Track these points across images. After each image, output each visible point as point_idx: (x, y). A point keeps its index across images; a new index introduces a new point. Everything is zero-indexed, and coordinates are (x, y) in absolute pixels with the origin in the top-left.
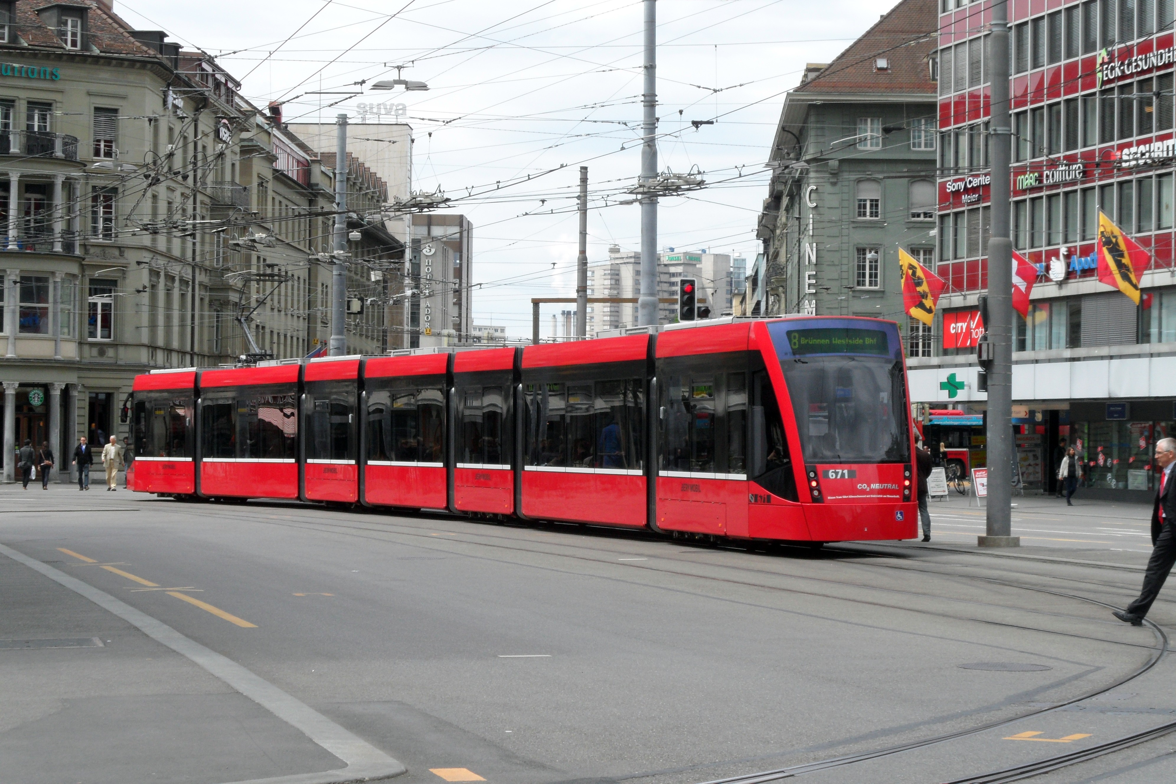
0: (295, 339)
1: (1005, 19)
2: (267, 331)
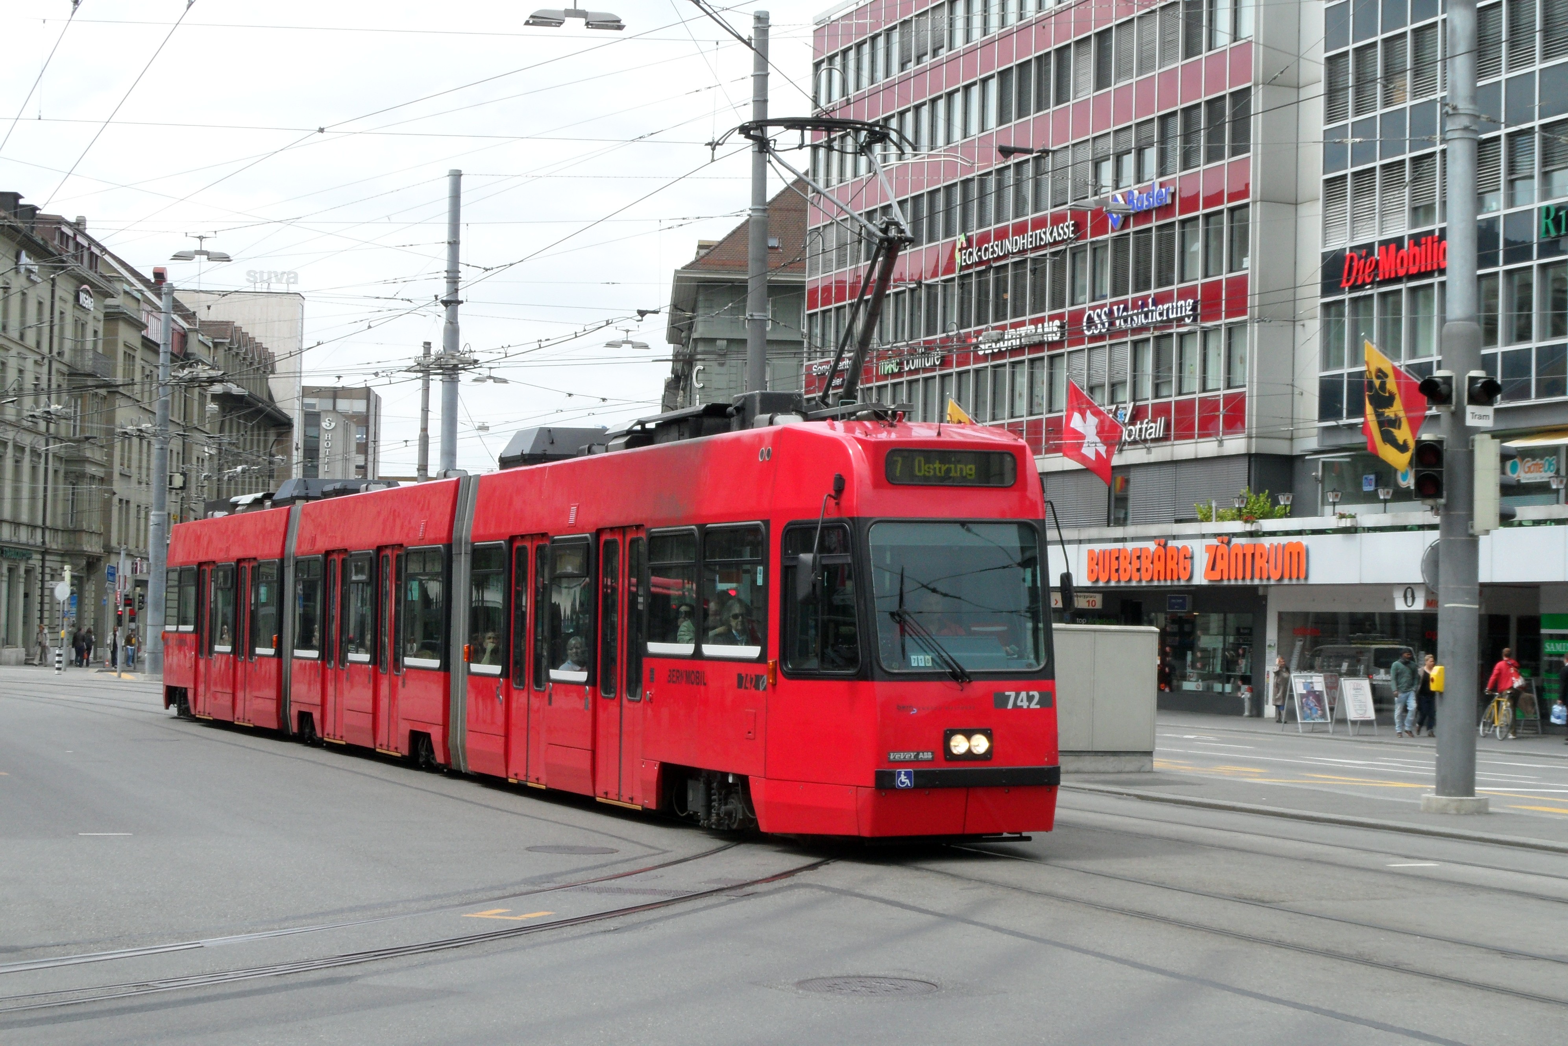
2: (133, 506)
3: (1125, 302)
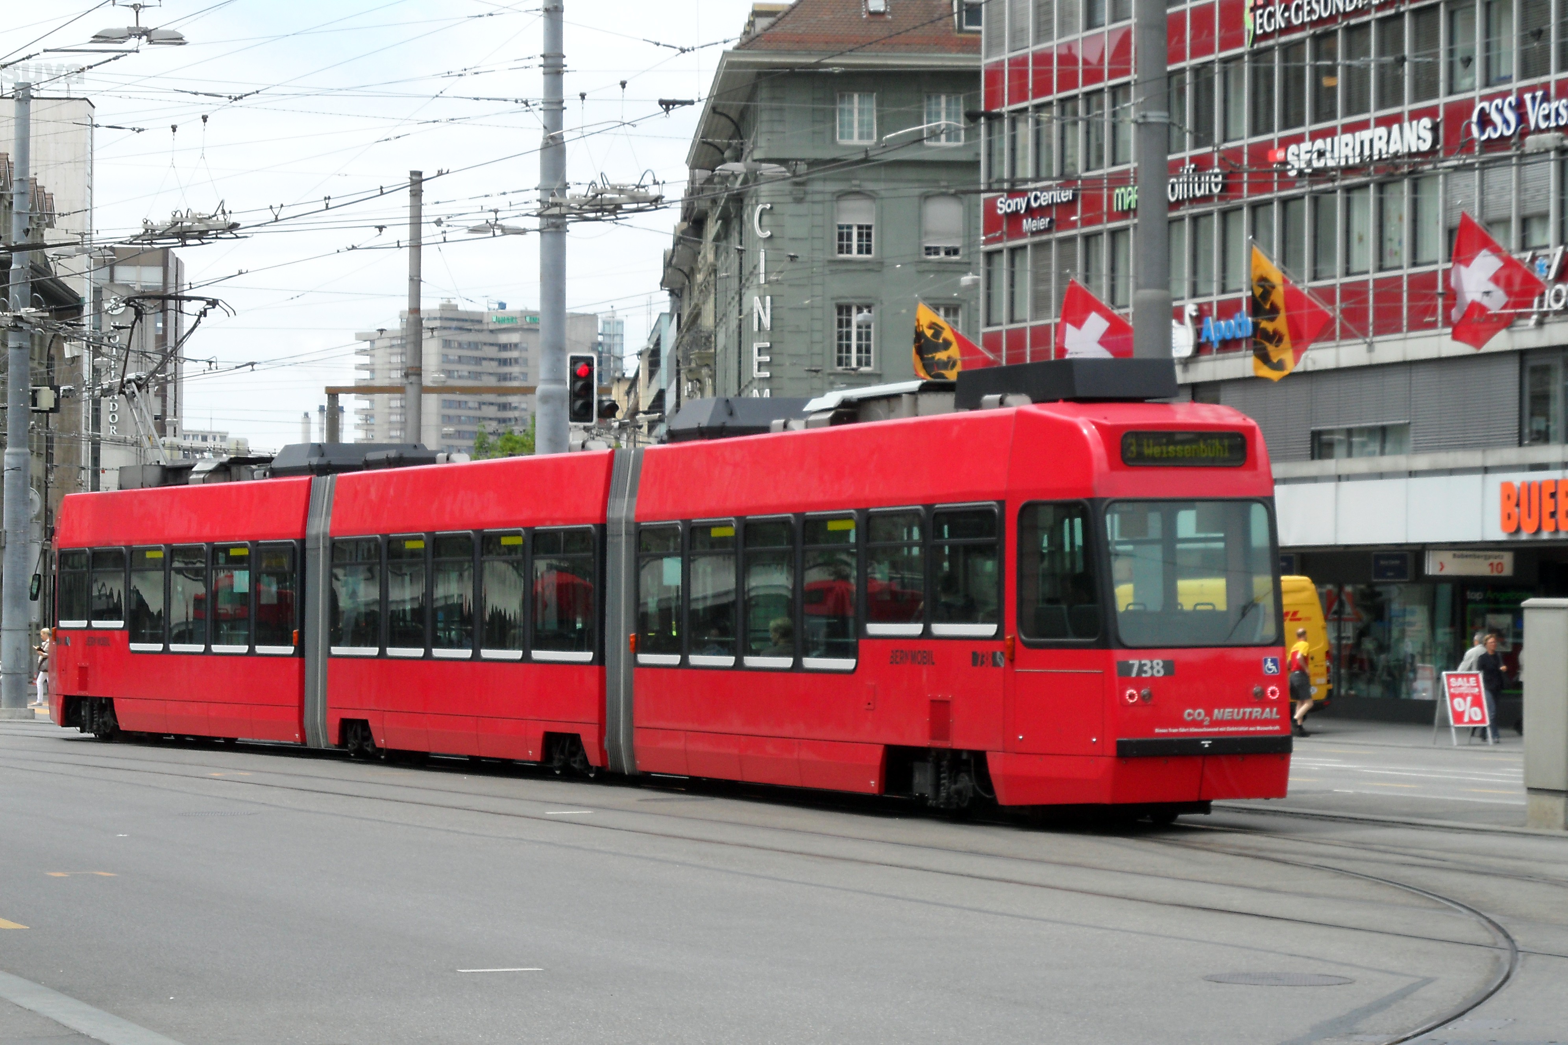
3: (1546, 87)
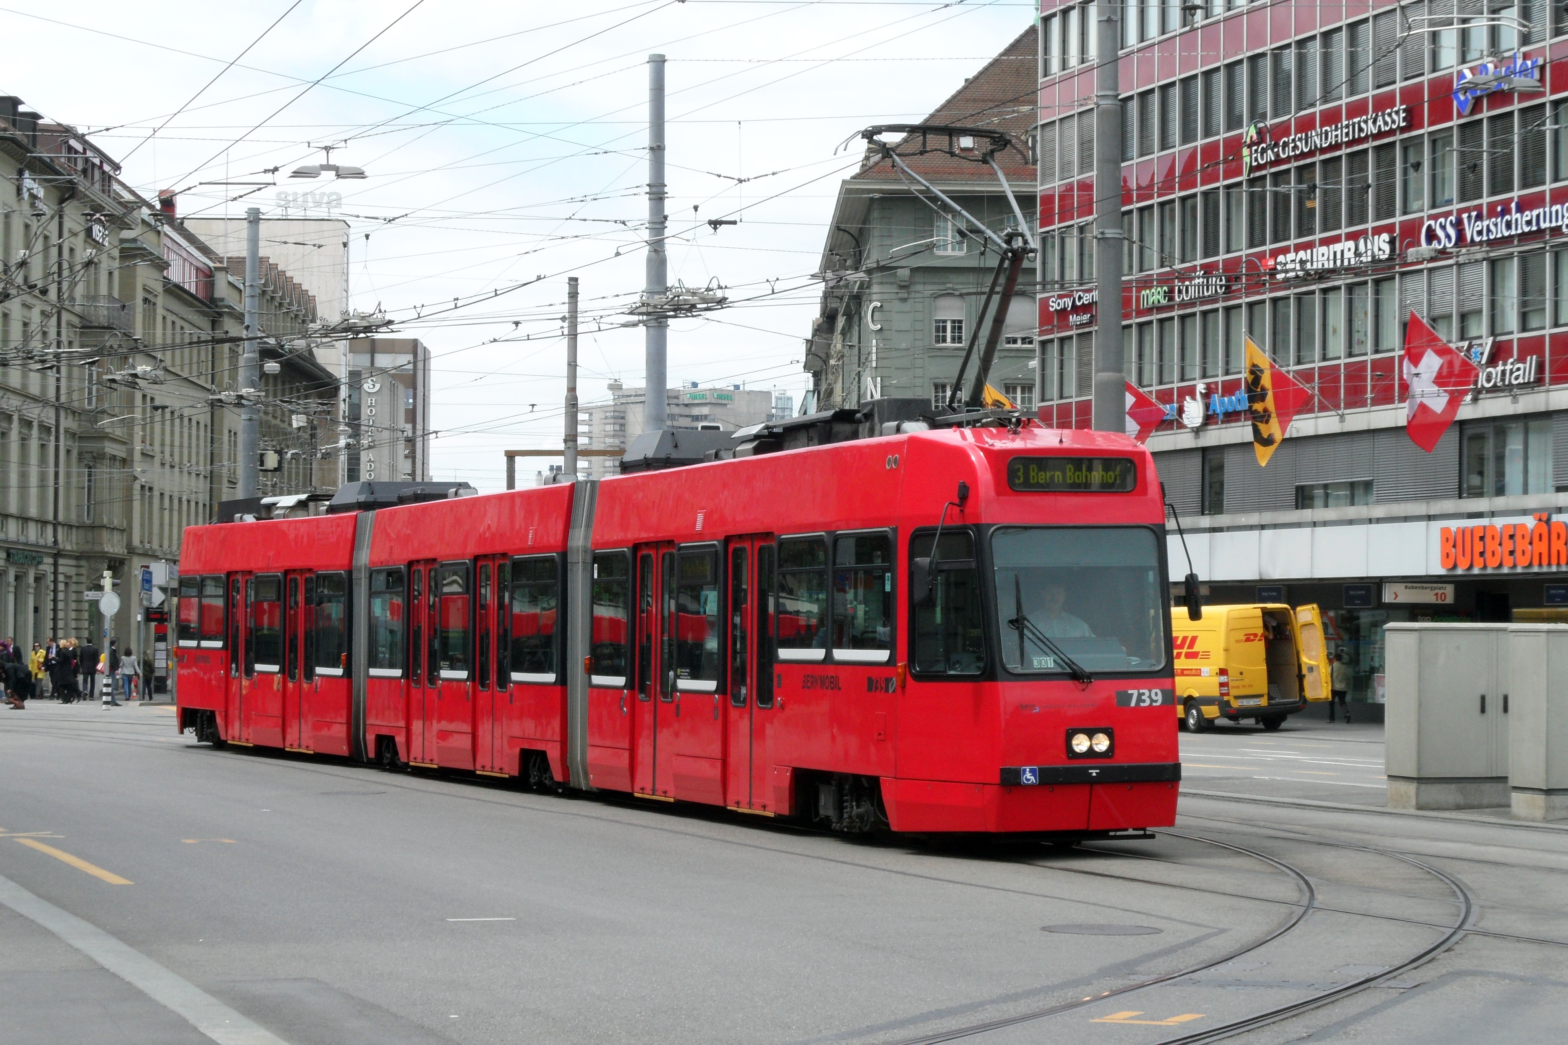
0: (193, 504)
1: (1116, 90)
2: (156, 493)
3: (1479, 208)
